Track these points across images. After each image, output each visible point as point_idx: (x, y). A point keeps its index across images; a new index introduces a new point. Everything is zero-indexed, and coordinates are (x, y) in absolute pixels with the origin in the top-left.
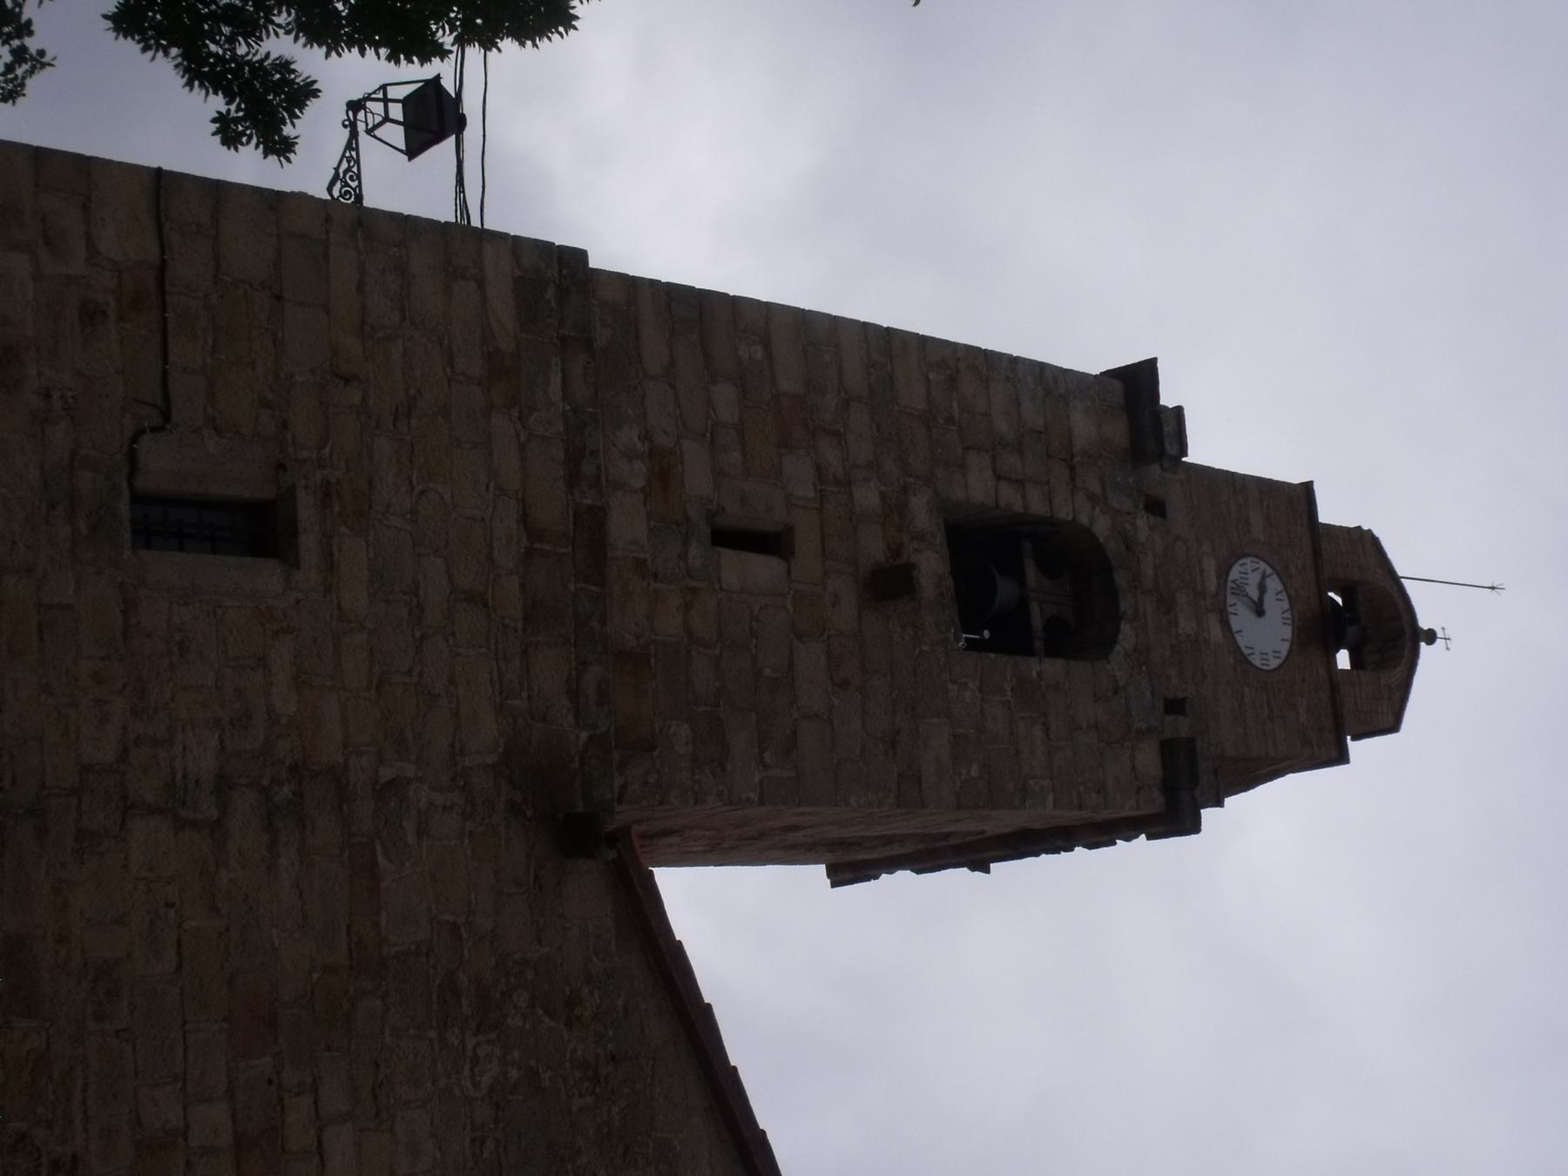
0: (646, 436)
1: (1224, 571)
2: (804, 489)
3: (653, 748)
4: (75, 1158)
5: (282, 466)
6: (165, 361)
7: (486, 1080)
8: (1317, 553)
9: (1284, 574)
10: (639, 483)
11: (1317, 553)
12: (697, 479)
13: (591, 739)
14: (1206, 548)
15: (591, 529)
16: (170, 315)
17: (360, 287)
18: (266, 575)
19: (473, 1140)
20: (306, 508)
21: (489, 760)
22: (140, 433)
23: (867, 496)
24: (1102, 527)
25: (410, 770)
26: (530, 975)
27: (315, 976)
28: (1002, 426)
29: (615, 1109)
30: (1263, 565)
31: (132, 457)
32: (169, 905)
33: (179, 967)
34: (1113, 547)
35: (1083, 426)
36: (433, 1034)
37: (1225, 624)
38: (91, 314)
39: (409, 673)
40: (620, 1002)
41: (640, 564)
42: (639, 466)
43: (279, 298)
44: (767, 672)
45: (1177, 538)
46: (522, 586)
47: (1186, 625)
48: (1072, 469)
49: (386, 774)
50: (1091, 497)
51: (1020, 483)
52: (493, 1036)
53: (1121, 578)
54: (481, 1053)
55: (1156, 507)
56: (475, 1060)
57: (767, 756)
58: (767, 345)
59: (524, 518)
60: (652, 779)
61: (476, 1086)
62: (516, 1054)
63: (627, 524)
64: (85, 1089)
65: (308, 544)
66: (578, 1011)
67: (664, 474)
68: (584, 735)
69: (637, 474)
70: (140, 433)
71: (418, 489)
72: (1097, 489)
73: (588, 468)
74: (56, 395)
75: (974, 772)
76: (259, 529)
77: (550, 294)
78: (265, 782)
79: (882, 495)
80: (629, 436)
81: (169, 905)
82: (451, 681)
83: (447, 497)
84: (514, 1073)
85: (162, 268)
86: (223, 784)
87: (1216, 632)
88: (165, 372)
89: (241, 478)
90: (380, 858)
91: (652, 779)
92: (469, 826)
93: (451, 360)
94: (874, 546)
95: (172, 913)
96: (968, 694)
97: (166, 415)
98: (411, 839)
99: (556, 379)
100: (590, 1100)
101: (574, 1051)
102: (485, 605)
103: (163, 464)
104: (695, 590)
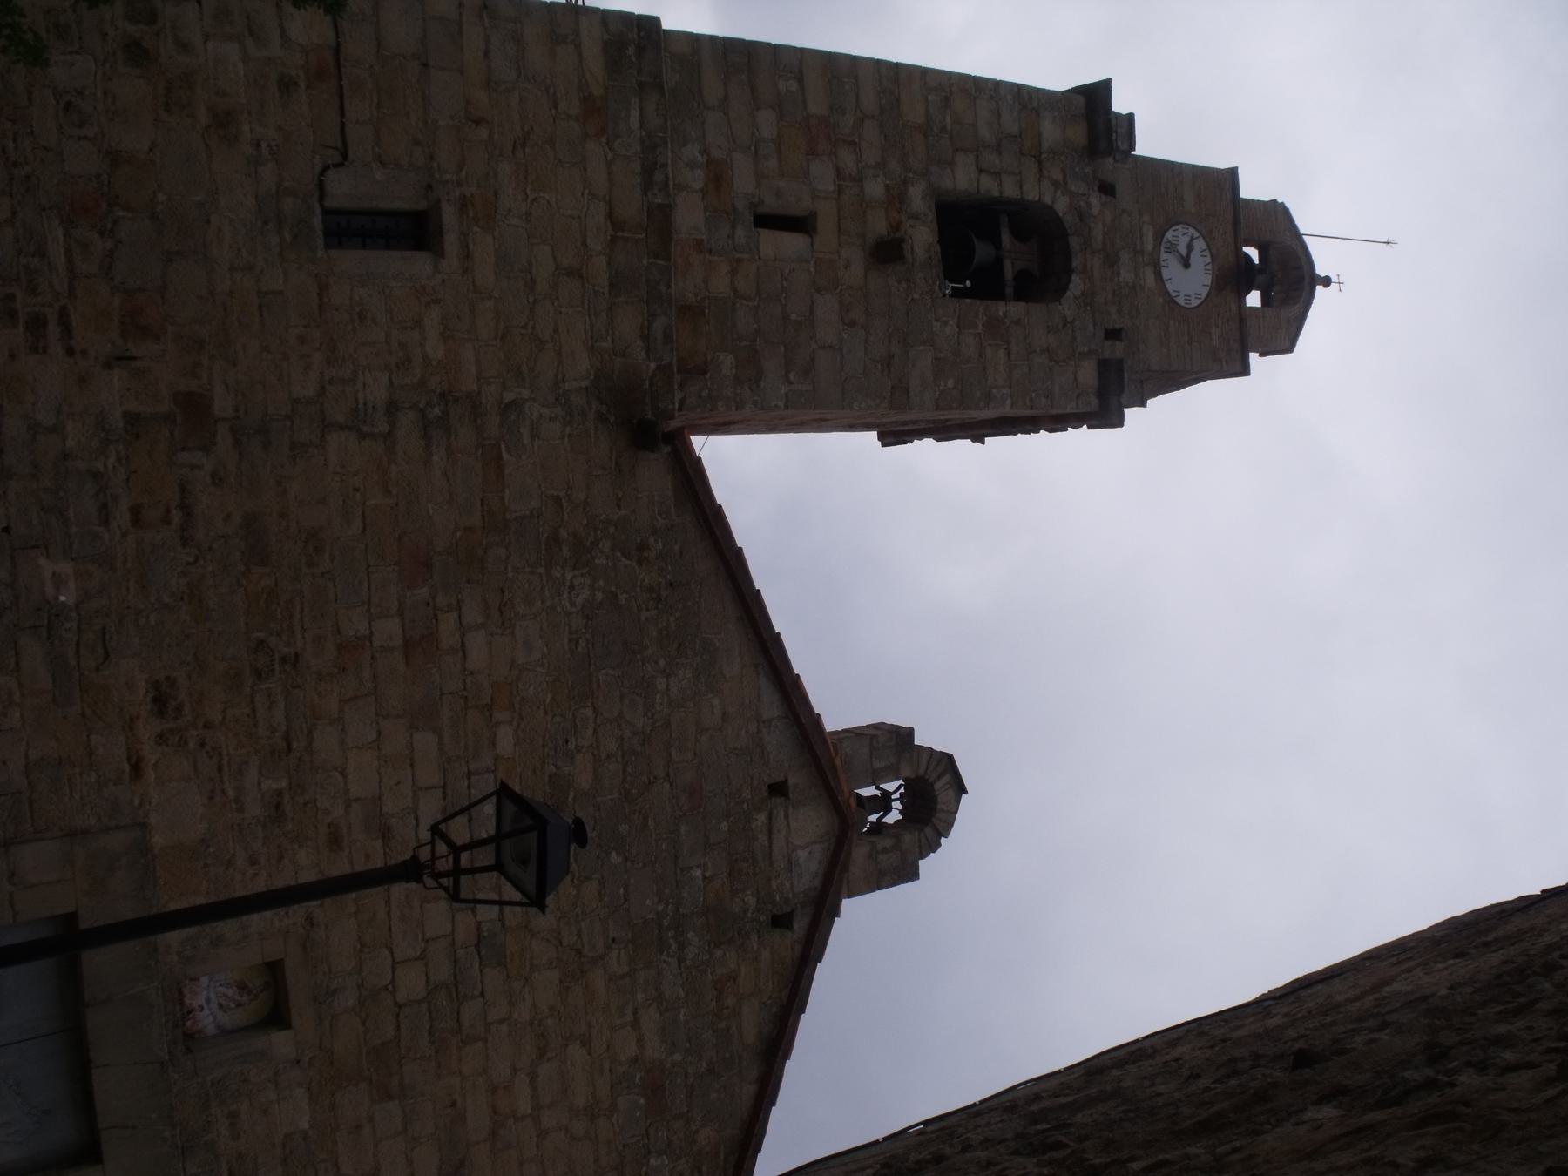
5: (430, 186)
6: (343, 115)
8: (1236, 222)
9: (1208, 237)
10: (698, 185)
12: (743, 180)
13: (658, 368)
14: (1146, 218)
15: (661, 220)
17: (486, 54)
18: (420, 263)
20: (449, 215)
21: (584, 384)
22: (325, 168)
23: (875, 188)
25: (526, 393)
26: (612, 530)
34: (1069, 220)
36: (542, 570)
37: (1158, 274)
39: (525, 327)
43: (425, 65)
44: (793, 316)
46: (609, 264)
47: (1126, 276)
48: (1040, 162)
53: (1075, 243)
56: (572, 587)
57: (792, 377)
59: (610, 215)
61: (573, 604)
65: (451, 241)
67: (717, 177)
68: (653, 365)
69: (696, 179)
70: (325, 168)
72: (1060, 178)
73: (658, 177)
75: (950, 383)
77: (631, 51)
80: (692, 151)
82: (556, 331)
84: (599, 596)
85: (337, 49)
86: (392, 408)
90: (505, 455)
92: (568, 430)
93: (556, 106)
94: (878, 226)
96: (948, 330)
97: (345, 156)
102: (581, 277)
103: (344, 189)
104: (739, 261)
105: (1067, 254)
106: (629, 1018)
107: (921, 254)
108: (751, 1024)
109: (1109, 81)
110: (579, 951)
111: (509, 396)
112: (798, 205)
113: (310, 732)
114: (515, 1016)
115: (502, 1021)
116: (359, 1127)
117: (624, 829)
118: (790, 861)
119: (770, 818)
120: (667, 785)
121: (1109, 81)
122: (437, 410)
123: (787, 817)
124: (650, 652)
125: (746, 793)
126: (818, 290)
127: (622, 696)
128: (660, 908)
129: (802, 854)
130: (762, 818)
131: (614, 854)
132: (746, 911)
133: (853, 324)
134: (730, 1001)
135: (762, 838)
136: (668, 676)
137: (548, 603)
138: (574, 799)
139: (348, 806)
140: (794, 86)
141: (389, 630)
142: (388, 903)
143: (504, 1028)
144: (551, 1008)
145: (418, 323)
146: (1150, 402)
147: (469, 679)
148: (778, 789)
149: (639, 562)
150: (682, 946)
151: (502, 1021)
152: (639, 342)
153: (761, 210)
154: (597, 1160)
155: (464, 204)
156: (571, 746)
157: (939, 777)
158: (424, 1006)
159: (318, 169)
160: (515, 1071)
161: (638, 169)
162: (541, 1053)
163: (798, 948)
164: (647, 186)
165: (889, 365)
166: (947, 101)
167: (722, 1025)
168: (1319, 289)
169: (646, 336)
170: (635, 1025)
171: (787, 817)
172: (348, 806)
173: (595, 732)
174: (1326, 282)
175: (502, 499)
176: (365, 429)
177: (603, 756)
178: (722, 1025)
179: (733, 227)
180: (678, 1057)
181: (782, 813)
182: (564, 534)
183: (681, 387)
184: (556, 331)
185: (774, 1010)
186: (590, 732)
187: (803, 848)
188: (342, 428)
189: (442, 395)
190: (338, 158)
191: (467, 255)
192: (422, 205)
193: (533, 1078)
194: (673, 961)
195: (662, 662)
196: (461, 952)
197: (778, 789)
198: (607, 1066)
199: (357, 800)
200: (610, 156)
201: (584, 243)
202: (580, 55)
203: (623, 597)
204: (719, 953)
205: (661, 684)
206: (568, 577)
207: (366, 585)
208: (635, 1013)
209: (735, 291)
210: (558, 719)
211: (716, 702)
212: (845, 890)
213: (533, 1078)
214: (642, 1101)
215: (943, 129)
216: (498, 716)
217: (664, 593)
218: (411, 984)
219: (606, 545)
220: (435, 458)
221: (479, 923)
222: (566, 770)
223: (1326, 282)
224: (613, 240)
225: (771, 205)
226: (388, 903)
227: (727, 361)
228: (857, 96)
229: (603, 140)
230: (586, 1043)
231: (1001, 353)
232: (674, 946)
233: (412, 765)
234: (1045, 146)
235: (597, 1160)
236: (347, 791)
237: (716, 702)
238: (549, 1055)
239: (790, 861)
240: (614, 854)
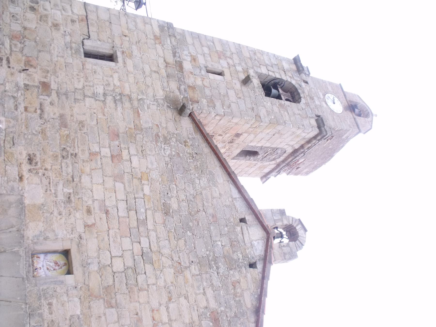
1: (324, 95)
2: (225, 65)
3: (198, 102)
4: (76, 154)
6: (88, 29)
9: (338, 98)
10: (189, 60)
12: (201, 61)
13: (184, 97)
14: (319, 90)
17: (127, 23)
19: (165, 164)
20: (119, 54)
21: (162, 98)
23: (239, 68)
24: (294, 82)
25: (145, 97)
26: (175, 136)
27: (127, 129)
28: (267, 62)
29: (198, 163)
30: (333, 96)
31: (83, 42)
32: (95, 113)
33: (97, 123)
34: (297, 86)
36: (154, 143)
38: (73, 21)
39: (143, 82)
40: (197, 144)
42: (188, 57)
44: (222, 93)
46: (166, 71)
47: (317, 102)
48: (285, 72)
49: (140, 97)
50: (290, 77)
53: (300, 91)
54: (166, 148)
56: (164, 149)
57: (224, 107)
58: (213, 43)
61: (165, 154)
62: (174, 150)
63: (187, 66)
64: (78, 142)
66: (187, 144)
67: (194, 59)
68: (182, 96)
70: (84, 39)
71: (142, 54)
73: (177, 55)
74: (67, 32)
75: (273, 117)
76: (111, 58)
77: (166, 28)
78: (114, 95)
80: (186, 52)
81: (95, 113)
82: (152, 84)
84: (174, 153)
85: (87, 16)
87: (325, 105)
88: (168, 312)
89: (106, 49)
90: (140, 111)
91: (199, 107)
92: (158, 108)
96: (268, 104)
97: (89, 37)
98: (146, 109)
99: (169, 41)
101: (187, 151)
102: (158, 73)
103: (90, 45)
104: (204, 78)
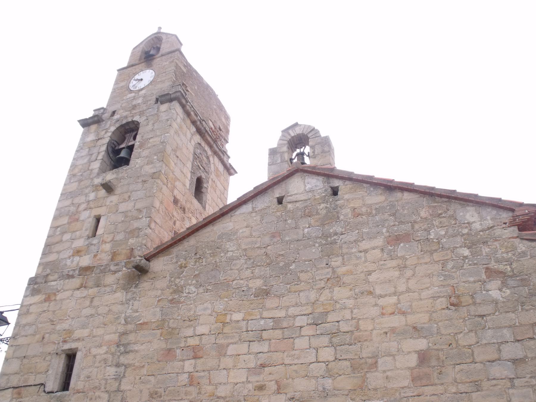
0: (69, 258)
1: (131, 92)
5: (57, 354)
6: (31, 385)
7: (194, 289)
8: (132, 66)
9: (135, 74)
10: (78, 258)
11: (132, 66)
12: (80, 243)
13: (125, 267)
14: (125, 98)
15: (85, 270)
16: (23, 385)
17: (26, 336)
18: (79, 356)
20: (67, 347)
21: (125, 293)
22: (44, 391)
23: (92, 196)
24: (113, 129)
25: (123, 315)
26: (173, 279)
27: (162, 338)
28: (86, 160)
29: (208, 252)
30: (132, 81)
31: (49, 393)
34: (118, 125)
35: (91, 137)
36: (181, 305)
37: (142, 89)
39: (104, 317)
40: (184, 253)
41: (95, 256)
43: (25, 357)
44: (123, 219)
45: (121, 106)
46: (92, 288)
47: (140, 101)
48: (99, 139)
50: (106, 133)
51: (99, 153)
52: (184, 288)
53: (124, 122)
54: (187, 291)
55: (114, 113)
56: (189, 293)
57: (140, 217)
58: (58, 227)
59: (78, 289)
60: (139, 248)
61: (195, 292)
63: (86, 261)
65: (73, 345)
66: (183, 265)
67: (78, 252)
68: (124, 269)
69: (77, 259)
70: (44, 391)
71: (68, 318)
72: (104, 131)
73: (71, 273)
75: (155, 157)
77: (36, 286)
79: (93, 192)
80: (69, 262)
82: (107, 305)
83: (71, 310)
84: (194, 282)
85: (14, 388)
86: (118, 365)
89: (59, 364)
90: (140, 322)
91: (139, 248)
92: (138, 299)
93: (45, 311)
94: (103, 192)
95: (142, 378)
96: (139, 162)
97: (42, 384)
98: (137, 314)
100: (204, 260)
101: (192, 265)
102: (93, 298)
103: (52, 384)
104: (103, 241)
105: (128, 123)
106: (362, 254)
107: (114, 176)
108: (377, 198)
109: (79, 121)
110: (328, 280)
111: (123, 322)
112: (90, 223)
113: (218, 397)
114: (351, 306)
115: (352, 312)
116: (387, 377)
117: (281, 264)
118: (310, 191)
119: (290, 202)
120: (269, 248)
121: (79, 121)
122: (121, 348)
123: (291, 196)
124: (218, 260)
125: (278, 214)
126: (117, 211)
127: (231, 269)
128: (317, 245)
129: (308, 187)
130: (290, 206)
131: (291, 268)
132: (326, 208)
133: (129, 197)
134: (364, 210)
135: (298, 205)
136: (228, 251)
137: (192, 302)
138: (266, 286)
139: (249, 382)
140: (59, 229)
141: (189, 365)
142: (291, 365)
143: (355, 311)
144: (351, 290)
145: (95, 356)
146: (323, 134)
147: (212, 332)
148: (280, 201)
149: (185, 267)
150: (336, 234)
151: (352, 312)
152: (116, 275)
153: (90, 235)
154: (426, 263)
155: (65, 341)
156: (245, 289)
157: (289, 135)
158: (338, 348)
159: (44, 394)
160: (376, 305)
161: (67, 280)
162: (370, 293)
163: (347, 182)
164: (72, 277)
165: (145, 181)
166: (74, 175)
167: (374, 212)
168: (162, 31)
169: (115, 272)
170: (366, 251)
171: (291, 196)
172: (249, 382)
173: (242, 279)
174: (160, 28)
175: (154, 322)
176: (122, 375)
177: (252, 275)
178: (374, 212)
179: (92, 244)
180: (384, 230)
181: (289, 198)
182: (170, 298)
183: (135, 257)
184: (107, 305)
185: (372, 189)
186: (242, 282)
187: (305, 186)
188: (120, 384)
189: (118, 346)
190: (43, 387)
191: (78, 340)
192: (63, 356)
193: (381, 296)
194: (341, 237)
195: (222, 255)
196: (318, 332)
197: (280, 201)
198: (382, 262)
199: (247, 378)
200: (62, 291)
201: (84, 297)
202: (33, 304)
203: (196, 272)
204: (342, 217)
205: (230, 254)
206: (185, 295)
207: (171, 374)
208: (361, 252)
209: (111, 241)
210: (234, 295)
211: (241, 231)
212: (328, 166)
213: (381, 296)
214: (402, 245)
215: (81, 175)
216: (228, 321)
217: (198, 256)
218: (327, 354)
219: (178, 280)
220: (136, 348)
221: (307, 324)
222: (254, 290)
223: (160, 28)
224: (85, 287)
225: (89, 232)
226: (291, 365)
227: (131, 241)
228: (66, 207)
229: (57, 293)
230: (369, 273)
231: (151, 140)
232: (335, 237)
233: (239, 355)
234: (94, 138)
235: (426, 263)
236: (243, 382)
237: (241, 231)
238: (372, 289)
239: (310, 191)
240: (291, 268)
